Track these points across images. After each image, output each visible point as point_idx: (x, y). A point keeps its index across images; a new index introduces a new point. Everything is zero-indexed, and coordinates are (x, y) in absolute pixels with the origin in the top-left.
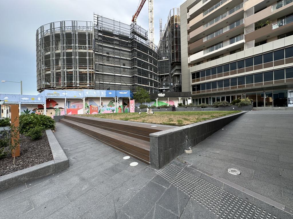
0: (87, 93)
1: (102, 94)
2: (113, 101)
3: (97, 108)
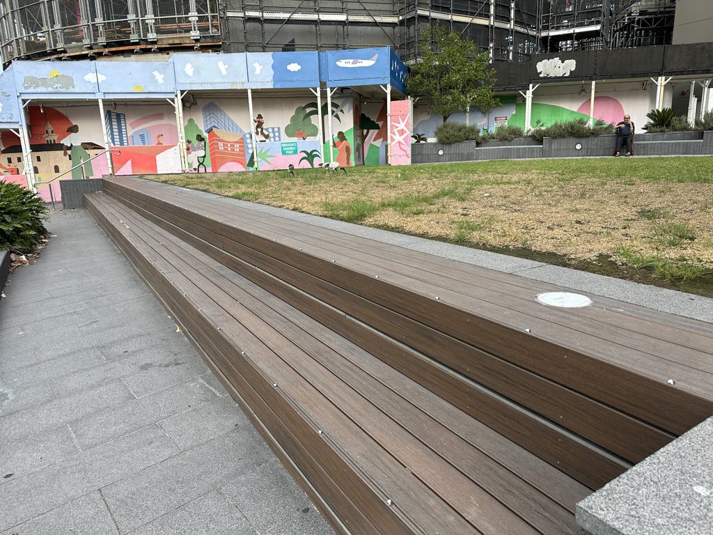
0: (189, 70)
1: (258, 72)
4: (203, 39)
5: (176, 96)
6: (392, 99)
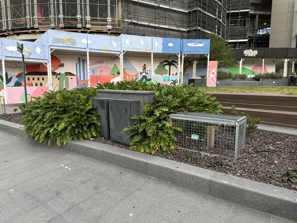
0: (127, 42)
1: (156, 45)
2: (165, 63)
3: (136, 75)
4: (112, 30)
5: (121, 53)
6: (210, 60)
